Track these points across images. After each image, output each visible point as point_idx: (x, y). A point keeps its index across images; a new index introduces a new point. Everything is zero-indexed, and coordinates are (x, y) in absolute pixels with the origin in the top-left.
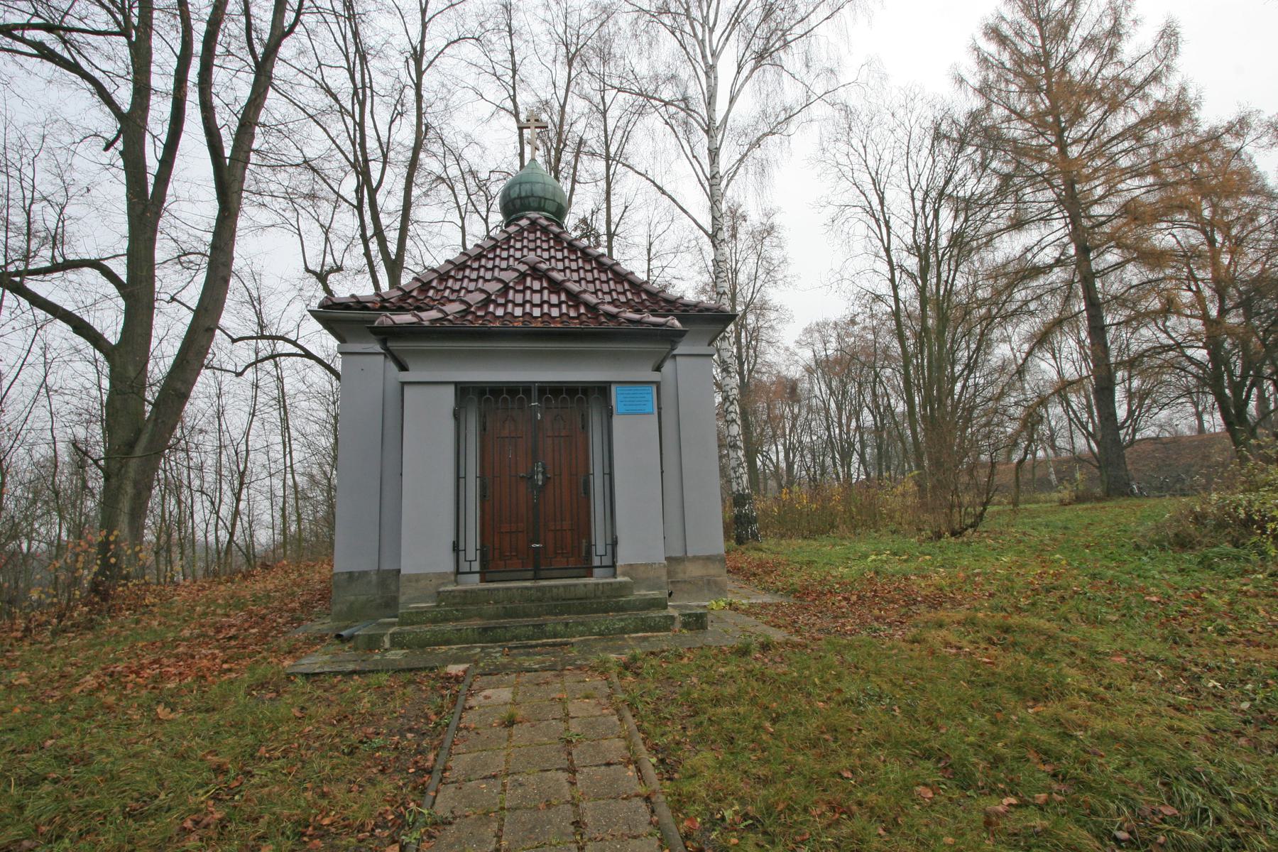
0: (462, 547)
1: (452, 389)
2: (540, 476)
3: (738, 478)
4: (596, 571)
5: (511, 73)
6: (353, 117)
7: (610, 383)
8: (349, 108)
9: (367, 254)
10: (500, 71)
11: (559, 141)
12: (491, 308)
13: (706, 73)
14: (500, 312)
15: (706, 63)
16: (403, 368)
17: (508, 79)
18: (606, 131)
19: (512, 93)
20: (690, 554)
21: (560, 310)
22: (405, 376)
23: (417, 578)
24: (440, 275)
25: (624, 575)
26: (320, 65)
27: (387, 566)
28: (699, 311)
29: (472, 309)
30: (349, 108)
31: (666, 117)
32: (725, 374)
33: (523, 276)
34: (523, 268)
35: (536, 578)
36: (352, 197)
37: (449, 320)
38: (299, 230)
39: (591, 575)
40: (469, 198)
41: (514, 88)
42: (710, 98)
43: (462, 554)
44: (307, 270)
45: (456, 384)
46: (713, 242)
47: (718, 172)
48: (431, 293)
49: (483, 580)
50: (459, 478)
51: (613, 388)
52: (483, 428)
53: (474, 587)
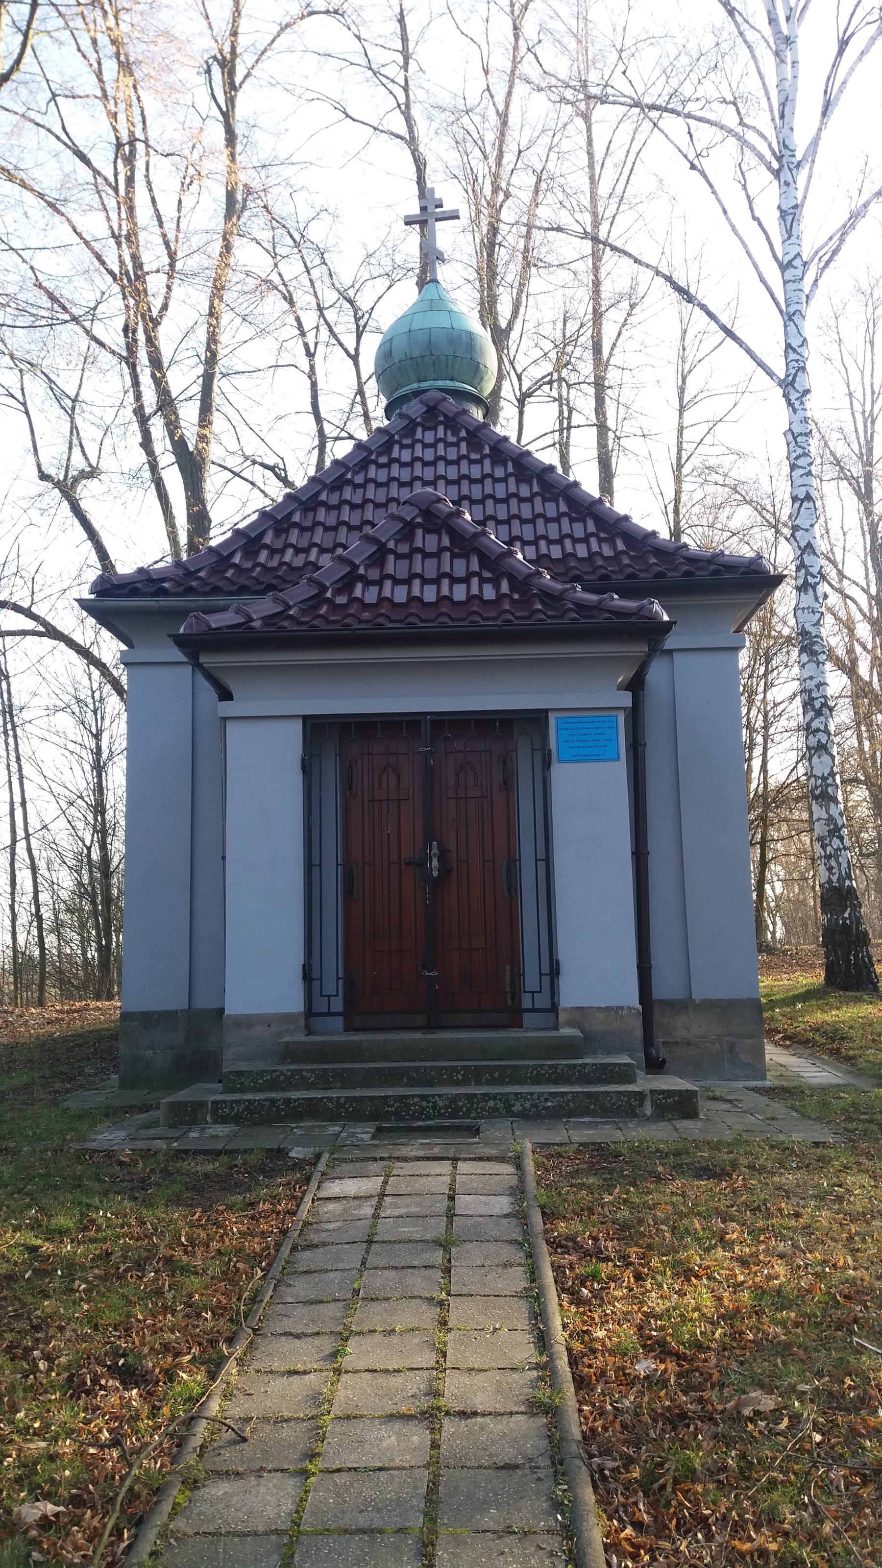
0: (316, 974)
1: (299, 724)
2: (435, 862)
3: (828, 857)
4: (526, 1016)
5: (400, 59)
6: (116, 190)
7: (546, 711)
8: (109, 173)
9: (147, 443)
10: (378, 57)
11: (496, 189)
12: (358, 592)
13: (777, 54)
14: (371, 596)
15: (777, 32)
16: (225, 695)
17: (393, 71)
18: (591, 155)
19: (402, 99)
20: (697, 996)
21: (468, 589)
22: (226, 708)
23: (246, 1022)
24: (277, 522)
25: (570, 1024)
26: (54, 95)
27: (204, 1002)
28: (716, 572)
29: (329, 594)
30: (109, 173)
31: (692, 156)
32: (805, 658)
33: (407, 531)
34: (409, 513)
35: (430, 1027)
36: (117, 341)
37: (292, 617)
38: (24, 404)
39: (517, 1023)
40: (322, 315)
41: (406, 89)
42: (783, 105)
43: (316, 984)
44: (44, 476)
45: (305, 718)
46: (786, 395)
47: (798, 255)
48: (263, 556)
49: (349, 1027)
50: (311, 866)
51: (552, 718)
52: (348, 785)
53: (336, 1038)
